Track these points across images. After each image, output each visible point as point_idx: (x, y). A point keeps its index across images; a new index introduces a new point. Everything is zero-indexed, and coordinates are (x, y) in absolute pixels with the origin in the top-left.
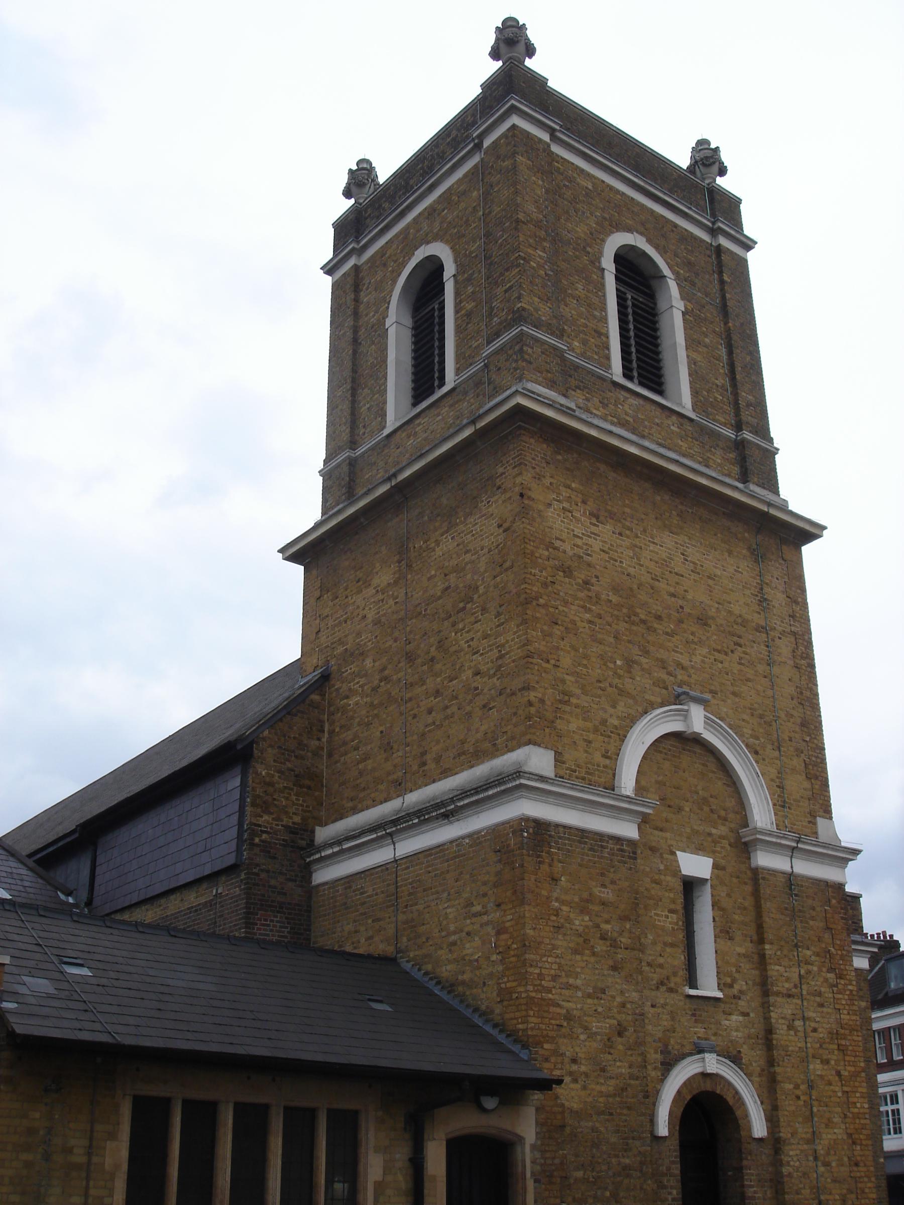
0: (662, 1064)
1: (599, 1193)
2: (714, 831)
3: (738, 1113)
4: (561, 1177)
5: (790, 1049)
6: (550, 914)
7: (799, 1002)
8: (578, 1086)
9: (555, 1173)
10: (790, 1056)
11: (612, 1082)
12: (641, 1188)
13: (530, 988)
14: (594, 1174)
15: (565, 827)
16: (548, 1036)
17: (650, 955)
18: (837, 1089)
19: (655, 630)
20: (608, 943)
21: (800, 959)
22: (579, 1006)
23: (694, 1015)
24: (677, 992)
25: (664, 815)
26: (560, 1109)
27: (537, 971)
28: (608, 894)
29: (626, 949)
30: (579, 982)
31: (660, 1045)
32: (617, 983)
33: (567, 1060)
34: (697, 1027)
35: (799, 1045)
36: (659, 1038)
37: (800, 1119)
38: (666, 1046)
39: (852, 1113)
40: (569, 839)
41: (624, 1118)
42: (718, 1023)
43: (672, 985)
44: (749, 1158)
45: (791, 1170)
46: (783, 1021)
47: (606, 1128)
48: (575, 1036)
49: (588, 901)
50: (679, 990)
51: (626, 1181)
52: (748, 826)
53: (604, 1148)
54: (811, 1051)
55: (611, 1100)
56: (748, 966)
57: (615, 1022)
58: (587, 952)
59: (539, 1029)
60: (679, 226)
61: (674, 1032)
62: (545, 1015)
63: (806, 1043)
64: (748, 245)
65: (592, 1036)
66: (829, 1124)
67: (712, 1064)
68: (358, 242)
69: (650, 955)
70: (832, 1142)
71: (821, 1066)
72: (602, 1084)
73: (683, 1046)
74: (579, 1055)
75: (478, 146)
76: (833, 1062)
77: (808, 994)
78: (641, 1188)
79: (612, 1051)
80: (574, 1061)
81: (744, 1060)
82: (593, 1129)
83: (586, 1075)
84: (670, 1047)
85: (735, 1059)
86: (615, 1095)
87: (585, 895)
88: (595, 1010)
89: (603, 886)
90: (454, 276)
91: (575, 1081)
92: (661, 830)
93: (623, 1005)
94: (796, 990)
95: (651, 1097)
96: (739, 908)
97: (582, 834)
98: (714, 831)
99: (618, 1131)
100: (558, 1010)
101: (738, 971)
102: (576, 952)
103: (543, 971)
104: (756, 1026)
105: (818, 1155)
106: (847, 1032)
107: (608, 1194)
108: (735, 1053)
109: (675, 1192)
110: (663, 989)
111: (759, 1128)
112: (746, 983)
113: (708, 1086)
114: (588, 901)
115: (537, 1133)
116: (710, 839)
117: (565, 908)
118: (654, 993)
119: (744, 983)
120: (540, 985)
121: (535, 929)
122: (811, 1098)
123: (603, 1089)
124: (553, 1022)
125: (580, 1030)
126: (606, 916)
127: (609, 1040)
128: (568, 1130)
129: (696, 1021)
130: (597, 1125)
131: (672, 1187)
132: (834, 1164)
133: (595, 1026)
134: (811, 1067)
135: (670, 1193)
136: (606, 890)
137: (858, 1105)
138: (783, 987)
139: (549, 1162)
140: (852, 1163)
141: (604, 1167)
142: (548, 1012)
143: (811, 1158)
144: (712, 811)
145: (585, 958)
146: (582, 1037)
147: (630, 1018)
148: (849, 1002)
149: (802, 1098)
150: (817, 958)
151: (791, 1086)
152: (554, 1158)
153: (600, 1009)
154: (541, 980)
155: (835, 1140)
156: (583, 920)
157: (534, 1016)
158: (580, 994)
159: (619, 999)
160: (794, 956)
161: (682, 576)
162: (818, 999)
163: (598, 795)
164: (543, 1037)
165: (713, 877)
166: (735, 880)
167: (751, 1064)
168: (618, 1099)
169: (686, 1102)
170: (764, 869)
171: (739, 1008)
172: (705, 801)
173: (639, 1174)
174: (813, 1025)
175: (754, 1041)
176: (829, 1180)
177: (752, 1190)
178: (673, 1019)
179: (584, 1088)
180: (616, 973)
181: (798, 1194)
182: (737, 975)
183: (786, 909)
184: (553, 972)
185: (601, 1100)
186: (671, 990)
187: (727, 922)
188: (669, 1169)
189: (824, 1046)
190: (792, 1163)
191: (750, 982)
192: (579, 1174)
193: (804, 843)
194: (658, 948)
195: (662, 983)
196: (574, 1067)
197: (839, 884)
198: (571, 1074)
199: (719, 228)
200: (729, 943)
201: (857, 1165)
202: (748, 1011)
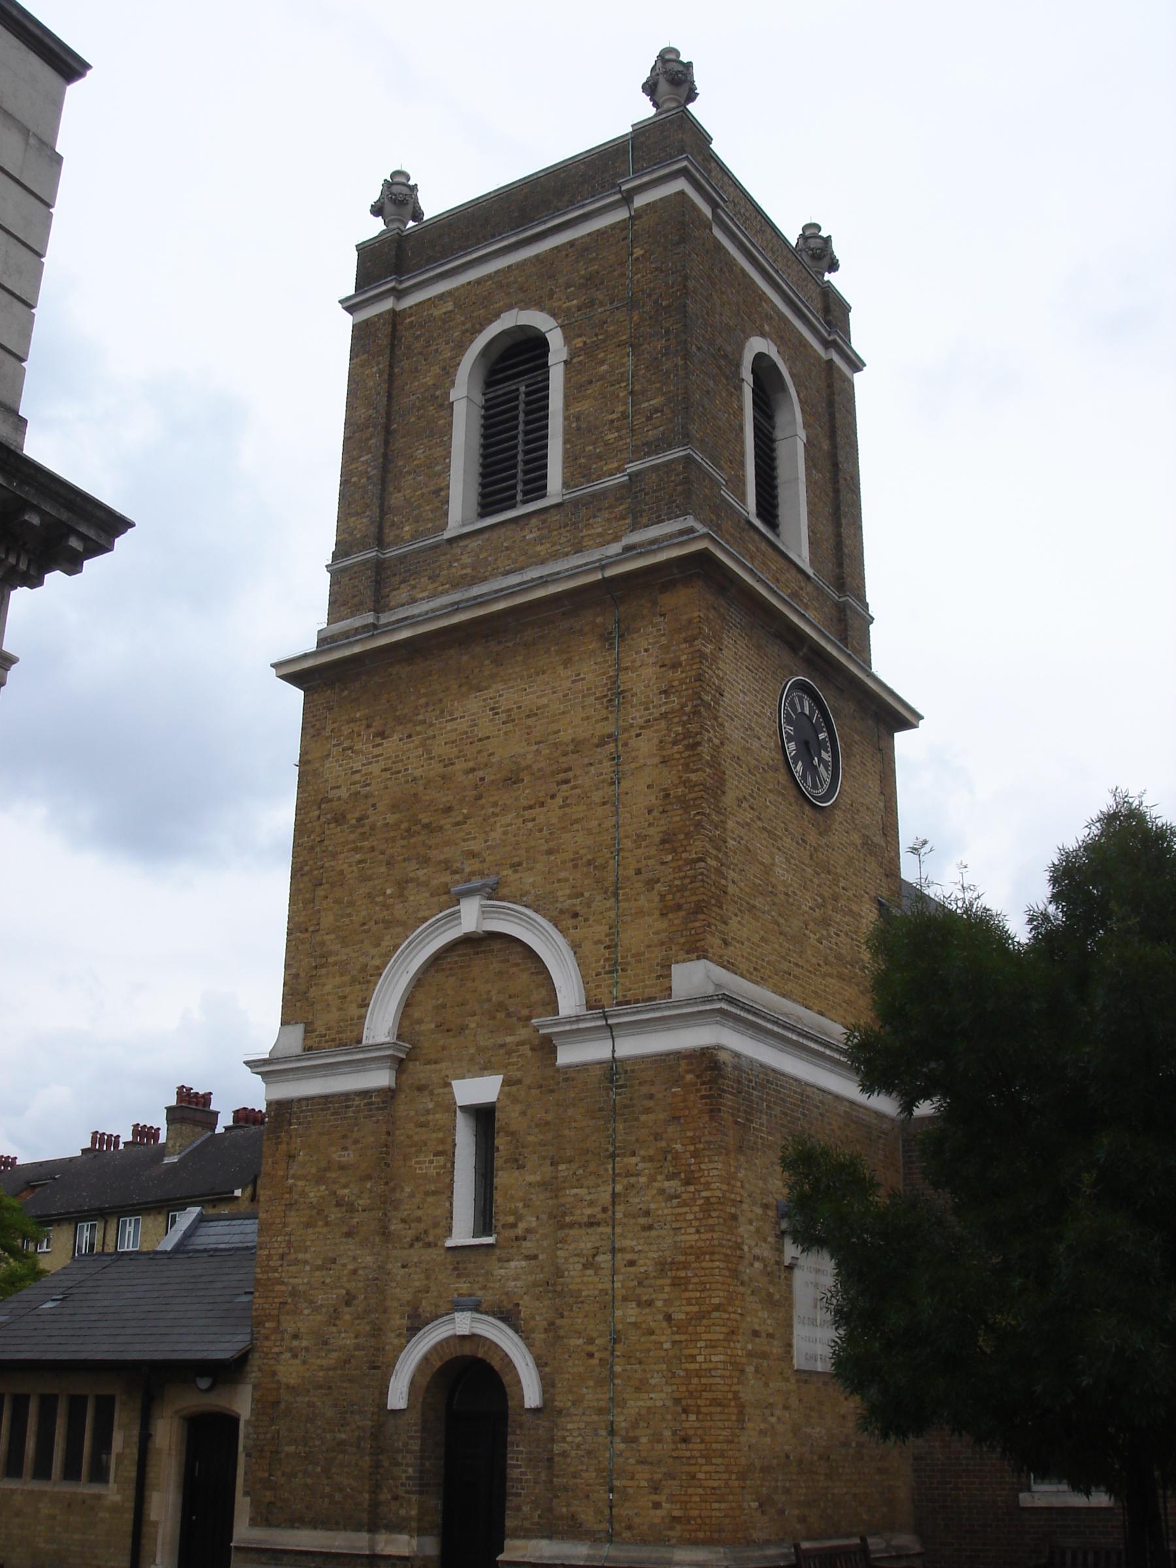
0: (408, 1329)
1: (310, 1468)
2: (509, 1039)
3: (506, 1379)
4: (271, 1452)
5: (584, 1294)
6: (283, 1194)
7: (608, 1230)
8: (298, 1361)
9: (266, 1448)
10: (582, 1302)
11: (335, 1355)
12: (357, 1465)
13: (258, 1270)
14: (307, 1449)
15: (307, 1099)
16: (270, 1315)
17: (405, 1210)
18: (663, 1338)
19: (441, 828)
20: (344, 1209)
21: (617, 1171)
22: (306, 1281)
23: (456, 1269)
24: (436, 1245)
25: (441, 1043)
26: (276, 1386)
27: (266, 1252)
28: (349, 1157)
29: (364, 1211)
30: (308, 1256)
31: (407, 1309)
32: (349, 1249)
33: (286, 1336)
34: (459, 1283)
35: (600, 1286)
36: (408, 1301)
37: (591, 1383)
38: (416, 1308)
39: (686, 1370)
40: (311, 1110)
41: (344, 1391)
42: (489, 1273)
43: (431, 1239)
44: (518, 1432)
45: (566, 1446)
46: (576, 1259)
47: (323, 1403)
48: (299, 1311)
49: (325, 1170)
50: (439, 1243)
51: (341, 1456)
52: (670, 996)
53: (319, 1423)
54: (620, 1293)
55: (331, 1373)
56: (542, 1197)
57: (344, 1292)
58: (320, 1223)
59: (263, 1309)
60: (575, 240)
61: (428, 1292)
62: (271, 1294)
63: (613, 1282)
64: (856, 364)
65: (317, 1309)
66: (641, 1387)
67: (463, 1323)
68: (401, 282)
69: (405, 1210)
70: (643, 1412)
71: (639, 1310)
72: (323, 1357)
73: (437, 1306)
74: (301, 1330)
75: (627, 199)
76: (659, 1304)
77: (625, 1216)
78: (357, 1465)
79: (338, 1322)
80: (296, 1336)
81: (522, 1315)
82: (311, 1405)
83: (307, 1349)
84: (420, 1310)
85: (509, 1316)
86: (335, 1369)
87: (323, 1164)
88: (323, 1282)
89: (345, 1149)
90: (565, 362)
91: (295, 1356)
92: (435, 1063)
93: (355, 1272)
94: (604, 1216)
95: (382, 1371)
96: (537, 1126)
97: (325, 1101)
98: (509, 1039)
99: (335, 1405)
100: (283, 1288)
101: (526, 1206)
102: (308, 1225)
103: (272, 1252)
104: (546, 1270)
105: (615, 1427)
106: (692, 1258)
107: (319, 1469)
108: (510, 1306)
109: (410, 1470)
110: (417, 1245)
111: (532, 1396)
112: (538, 1218)
113: (467, 1350)
114: (325, 1170)
115: (252, 1410)
116: (502, 1051)
117: (300, 1183)
118: (406, 1252)
119: (534, 1219)
120: (267, 1265)
121: (267, 1211)
122: (612, 1354)
123: (324, 1362)
124: (277, 1300)
125: (305, 1305)
126: (343, 1180)
127: (335, 1311)
128: (283, 1406)
129: (459, 1276)
130: (315, 1399)
131: (407, 1465)
132: (644, 1440)
133: (320, 1298)
134: (618, 1313)
135: (405, 1472)
136: (346, 1153)
137: (700, 1358)
138: (582, 1214)
139: (262, 1437)
140: (677, 1438)
141: (317, 1443)
142: (272, 1291)
143: (603, 1433)
144: (509, 1015)
145: (317, 1230)
146: (306, 1312)
147: (361, 1285)
148: (700, 1215)
149: (596, 1355)
150: (648, 1165)
151: (580, 1342)
152: (266, 1433)
153: (328, 1280)
154: (269, 1261)
155: (649, 1408)
156: (319, 1191)
157: (259, 1297)
158: (308, 1268)
159: (351, 1267)
160: (607, 1170)
161: (488, 738)
162: (642, 1221)
163: (322, 1057)
164: (266, 1316)
165: (501, 1098)
166: (534, 1092)
167: (533, 1318)
168: (339, 1372)
169: (435, 1370)
170: (629, 1058)
171: (523, 1251)
172: (501, 1006)
173: (354, 1449)
174: (628, 1256)
175: (541, 1289)
176: (632, 1461)
177: (519, 1470)
178: (428, 1278)
179: (304, 1362)
180: (350, 1239)
181: (575, 1477)
182: (524, 1211)
183: (601, 1109)
184: (281, 1251)
185: (321, 1374)
186: (428, 1245)
187: (517, 1148)
188: (406, 1445)
189: (645, 1283)
190: (569, 1439)
191: (544, 1217)
192: (291, 1449)
193: (613, 1016)
194: (417, 1200)
195: (418, 1239)
196: (295, 1343)
197: (702, 1049)
198: (291, 1350)
199: (834, 341)
200: (516, 1173)
201: (685, 1440)
202: (536, 1252)
